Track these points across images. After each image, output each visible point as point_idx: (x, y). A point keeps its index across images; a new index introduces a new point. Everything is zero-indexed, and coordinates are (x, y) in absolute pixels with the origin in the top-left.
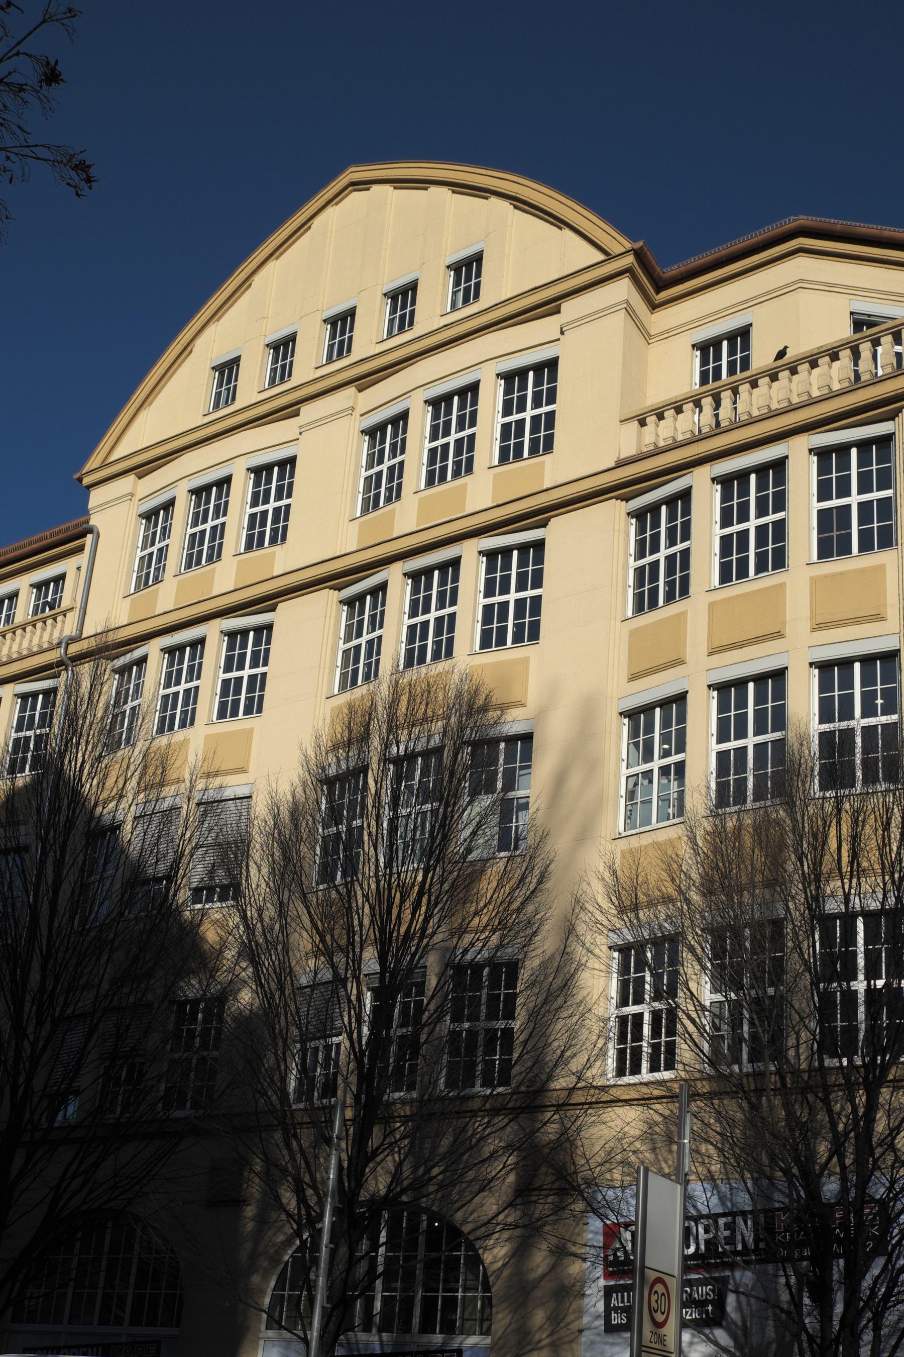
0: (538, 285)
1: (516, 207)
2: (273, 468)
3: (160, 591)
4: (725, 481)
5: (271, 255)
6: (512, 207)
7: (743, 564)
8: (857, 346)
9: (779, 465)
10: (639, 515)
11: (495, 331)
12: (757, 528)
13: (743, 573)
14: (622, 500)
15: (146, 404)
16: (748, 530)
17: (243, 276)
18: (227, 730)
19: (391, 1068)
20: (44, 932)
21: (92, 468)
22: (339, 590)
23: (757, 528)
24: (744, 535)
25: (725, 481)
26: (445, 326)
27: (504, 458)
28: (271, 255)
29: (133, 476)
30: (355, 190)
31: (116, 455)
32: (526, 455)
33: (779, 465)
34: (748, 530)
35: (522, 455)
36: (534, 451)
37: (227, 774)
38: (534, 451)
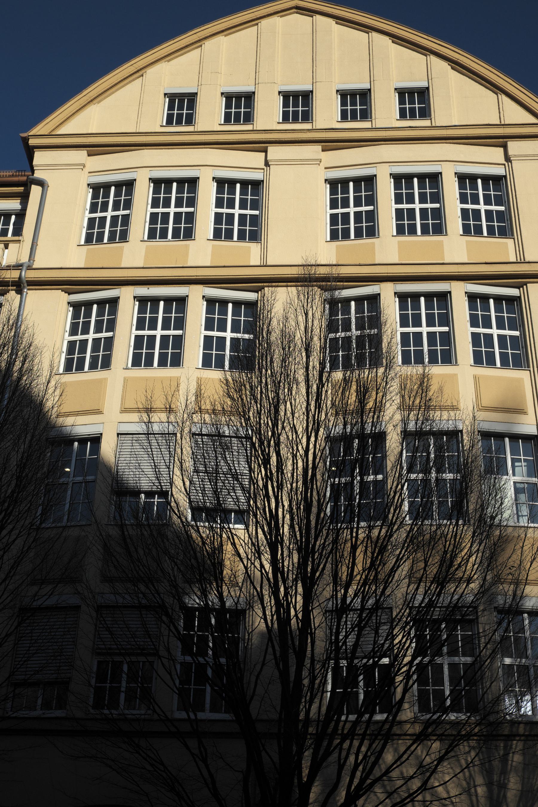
0: (491, 123)
1: (453, 68)
2: (172, 183)
3: (125, 249)
4: (142, 301)
5: (222, 31)
6: (450, 67)
7: (81, 361)
8: (8, 244)
9: (114, 302)
10: (76, 306)
11: (450, 143)
12: (93, 339)
13: (80, 368)
14: (65, 292)
15: (94, 102)
16: (88, 340)
17: (195, 38)
18: (90, 378)
19: (291, 685)
20: (396, 501)
21: (38, 134)
22: (69, 294)
23: (93, 339)
24: (84, 343)
25: (142, 301)
26: (410, 127)
27: (152, 235)
28: (222, 31)
29: (320, 147)
30: (297, 13)
31: (62, 131)
32: (106, 240)
33: (182, 301)
34: (88, 340)
35: (103, 241)
36: (112, 239)
37: (68, 416)
38: (112, 239)
